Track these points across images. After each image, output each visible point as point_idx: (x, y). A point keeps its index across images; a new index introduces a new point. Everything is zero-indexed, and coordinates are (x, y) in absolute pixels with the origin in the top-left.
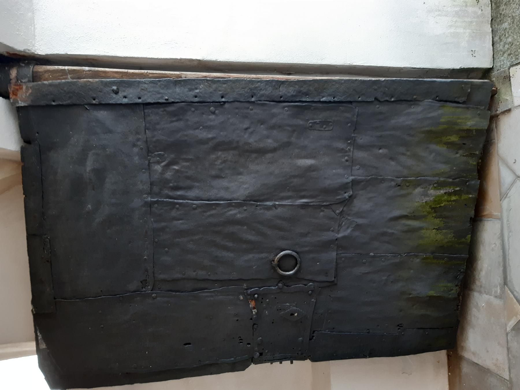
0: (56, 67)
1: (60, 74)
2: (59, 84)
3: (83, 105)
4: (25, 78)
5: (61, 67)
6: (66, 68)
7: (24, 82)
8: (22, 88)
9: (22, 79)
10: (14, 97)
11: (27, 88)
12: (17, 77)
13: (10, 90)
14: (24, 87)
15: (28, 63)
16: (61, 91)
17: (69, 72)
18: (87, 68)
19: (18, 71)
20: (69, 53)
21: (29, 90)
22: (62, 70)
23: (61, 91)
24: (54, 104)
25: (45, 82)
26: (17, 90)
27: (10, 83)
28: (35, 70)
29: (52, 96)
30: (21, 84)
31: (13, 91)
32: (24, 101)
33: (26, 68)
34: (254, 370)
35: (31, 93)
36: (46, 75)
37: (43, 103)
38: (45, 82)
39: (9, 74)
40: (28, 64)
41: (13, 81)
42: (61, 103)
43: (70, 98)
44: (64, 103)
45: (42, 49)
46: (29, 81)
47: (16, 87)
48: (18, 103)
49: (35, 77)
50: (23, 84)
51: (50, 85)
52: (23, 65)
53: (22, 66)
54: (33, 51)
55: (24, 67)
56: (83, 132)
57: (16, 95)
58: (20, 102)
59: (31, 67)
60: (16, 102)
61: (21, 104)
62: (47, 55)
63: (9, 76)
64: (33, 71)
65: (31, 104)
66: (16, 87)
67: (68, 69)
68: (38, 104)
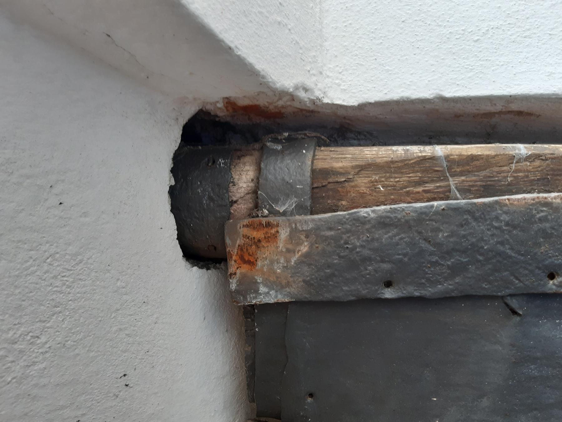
0: (399, 151)
1: (415, 176)
2: (422, 215)
3: (502, 297)
4: (288, 196)
5: (416, 150)
6: (440, 150)
7: (284, 214)
8: (275, 236)
9: (276, 201)
10: (245, 269)
11: (294, 233)
12: (255, 192)
13: (233, 245)
14: (284, 234)
15: (289, 139)
16: (424, 245)
17: (449, 168)
18: (522, 149)
19: (259, 170)
20: (449, 93)
21: (299, 244)
22: (424, 159)
23: (424, 245)
24: (389, 294)
25: (363, 212)
26: (257, 243)
27: (229, 216)
28: (320, 165)
29: (386, 266)
30: (272, 219)
31: (241, 248)
32: (276, 284)
33: (288, 161)
34: (172, 217)
35: (307, 255)
36: (362, 183)
37: (345, 291)
38: (363, 212)
39: (225, 184)
40: (293, 144)
41: (242, 208)
42: (417, 294)
43: (456, 270)
44: (429, 291)
45: (345, 81)
46: (301, 209)
47: (256, 234)
48: (257, 291)
49: (324, 192)
50: (280, 219)
51: (383, 223)
52: (279, 147)
53: (276, 152)
54: (318, 93)
55: (282, 152)
56: (485, 402)
57: (252, 264)
58: (263, 289)
59: (308, 155)
60: (248, 285)
61: (268, 295)
62: (362, 107)
63: (228, 191)
64: (313, 171)
65: (306, 296)
66: (256, 234)
67: (447, 158)
68: (328, 296)
